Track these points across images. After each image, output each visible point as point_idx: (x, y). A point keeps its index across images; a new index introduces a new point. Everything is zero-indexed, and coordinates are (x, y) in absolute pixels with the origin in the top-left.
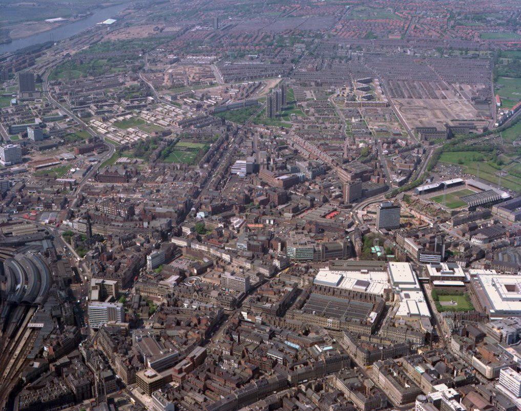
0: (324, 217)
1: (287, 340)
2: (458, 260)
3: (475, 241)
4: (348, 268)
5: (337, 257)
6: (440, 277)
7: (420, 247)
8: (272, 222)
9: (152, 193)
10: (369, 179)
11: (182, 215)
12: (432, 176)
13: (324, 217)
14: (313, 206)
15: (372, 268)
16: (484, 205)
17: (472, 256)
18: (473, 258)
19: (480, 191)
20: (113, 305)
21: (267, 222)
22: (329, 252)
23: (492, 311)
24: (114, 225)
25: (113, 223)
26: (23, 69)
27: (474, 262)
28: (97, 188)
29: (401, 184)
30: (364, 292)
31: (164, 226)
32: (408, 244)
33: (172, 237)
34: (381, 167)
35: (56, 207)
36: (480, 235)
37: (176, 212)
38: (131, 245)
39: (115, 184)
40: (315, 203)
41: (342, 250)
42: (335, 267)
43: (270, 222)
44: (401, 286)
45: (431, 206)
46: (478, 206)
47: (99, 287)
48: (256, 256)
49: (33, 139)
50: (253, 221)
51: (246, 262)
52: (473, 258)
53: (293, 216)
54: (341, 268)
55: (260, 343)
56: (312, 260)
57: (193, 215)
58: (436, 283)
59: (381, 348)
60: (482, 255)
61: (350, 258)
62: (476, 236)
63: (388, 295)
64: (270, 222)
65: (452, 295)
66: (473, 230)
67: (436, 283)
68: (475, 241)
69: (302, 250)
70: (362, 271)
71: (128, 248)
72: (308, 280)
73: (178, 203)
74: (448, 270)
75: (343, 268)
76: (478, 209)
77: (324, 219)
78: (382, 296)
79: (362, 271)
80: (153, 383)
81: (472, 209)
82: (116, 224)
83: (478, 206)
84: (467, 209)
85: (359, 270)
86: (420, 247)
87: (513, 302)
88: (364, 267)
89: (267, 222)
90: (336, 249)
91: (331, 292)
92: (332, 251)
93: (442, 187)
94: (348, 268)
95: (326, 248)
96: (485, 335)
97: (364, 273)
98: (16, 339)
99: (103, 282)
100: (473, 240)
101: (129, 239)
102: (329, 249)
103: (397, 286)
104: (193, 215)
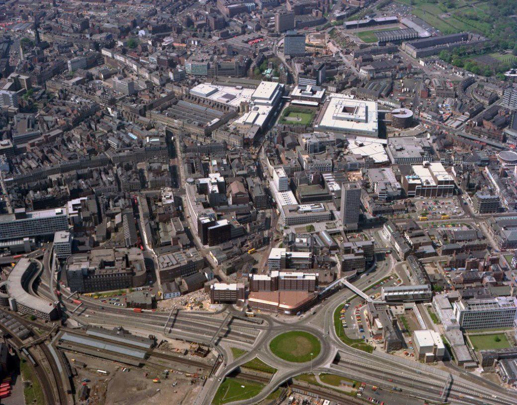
0: (247, 42)
1: (132, 132)
4: (229, 84)
5: (229, 75)
6: (299, 97)
8: (196, 43)
9: (118, 12)
10: (311, 12)
11: (124, 32)
13: (247, 42)
14: (244, 33)
15: (247, 86)
18: (348, 85)
19: (406, 27)
20: (8, 93)
21: (193, 43)
22: (222, 70)
24: (64, 36)
25: (63, 34)
28: (74, 6)
30: (225, 103)
31: (103, 39)
33: (103, 47)
35: (31, 19)
37: (119, 28)
38: (66, 52)
39: (90, 3)
40: (246, 30)
41: (234, 69)
42: (218, 82)
43: (194, 42)
44: (256, 101)
46: (388, 42)
47: (13, 80)
48: (160, 68)
50: (180, 41)
51: (146, 72)
52: (348, 85)
53: (219, 40)
54: (222, 83)
55: (108, 132)
56: (206, 76)
57: (135, 32)
59: (199, 145)
61: (243, 77)
63: (243, 107)
64: (194, 42)
65: (304, 113)
69: (197, 66)
71: (62, 55)
72: (186, 90)
73: (127, 21)
75: (224, 83)
76: (388, 45)
77: (247, 44)
80: (128, 220)
81: (382, 43)
82: (66, 35)
85: (235, 86)
87: (341, 121)
88: (239, 84)
89: (193, 43)
90: (229, 68)
91: (197, 101)
92: (225, 70)
93: (373, 23)
94: (229, 84)
95: (219, 66)
97: (238, 89)
98: (436, 389)
99: (19, 76)
101: (67, 47)
102: (222, 68)
104: (135, 32)
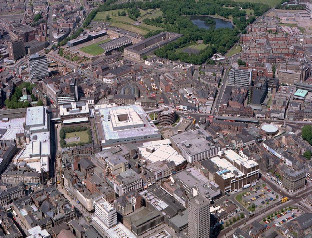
2: (88, 99)
3: (107, 81)
7: (58, 91)
12: (85, 31)
16: (117, 49)
17: (100, 93)
23: (103, 142)
26: (52, 237)
27: (103, 99)
29: (60, 40)
32: (49, 89)
34: (48, 28)
36: (110, 75)
44: (31, 129)
45: (78, 55)
49: (212, 160)
52: (101, 95)
58: (65, 122)
60: (109, 91)
62: (107, 76)
66: (106, 70)
67: (65, 122)
68: (107, 81)
70: (4, 119)
74: (76, 109)
76: (112, 53)
78: (15, 141)
79: (4, 119)
81: (109, 53)
83: (112, 50)
84: (105, 55)
86: (58, 91)
96: (94, 166)
97: (5, 121)
100: (104, 80)
103: (28, 129)
